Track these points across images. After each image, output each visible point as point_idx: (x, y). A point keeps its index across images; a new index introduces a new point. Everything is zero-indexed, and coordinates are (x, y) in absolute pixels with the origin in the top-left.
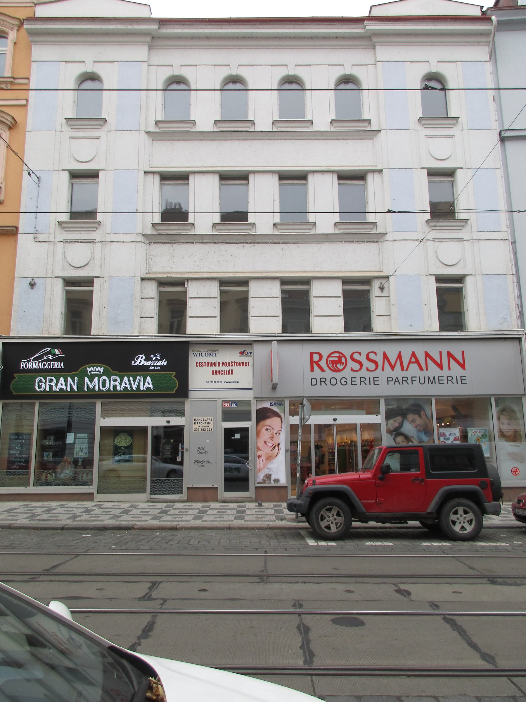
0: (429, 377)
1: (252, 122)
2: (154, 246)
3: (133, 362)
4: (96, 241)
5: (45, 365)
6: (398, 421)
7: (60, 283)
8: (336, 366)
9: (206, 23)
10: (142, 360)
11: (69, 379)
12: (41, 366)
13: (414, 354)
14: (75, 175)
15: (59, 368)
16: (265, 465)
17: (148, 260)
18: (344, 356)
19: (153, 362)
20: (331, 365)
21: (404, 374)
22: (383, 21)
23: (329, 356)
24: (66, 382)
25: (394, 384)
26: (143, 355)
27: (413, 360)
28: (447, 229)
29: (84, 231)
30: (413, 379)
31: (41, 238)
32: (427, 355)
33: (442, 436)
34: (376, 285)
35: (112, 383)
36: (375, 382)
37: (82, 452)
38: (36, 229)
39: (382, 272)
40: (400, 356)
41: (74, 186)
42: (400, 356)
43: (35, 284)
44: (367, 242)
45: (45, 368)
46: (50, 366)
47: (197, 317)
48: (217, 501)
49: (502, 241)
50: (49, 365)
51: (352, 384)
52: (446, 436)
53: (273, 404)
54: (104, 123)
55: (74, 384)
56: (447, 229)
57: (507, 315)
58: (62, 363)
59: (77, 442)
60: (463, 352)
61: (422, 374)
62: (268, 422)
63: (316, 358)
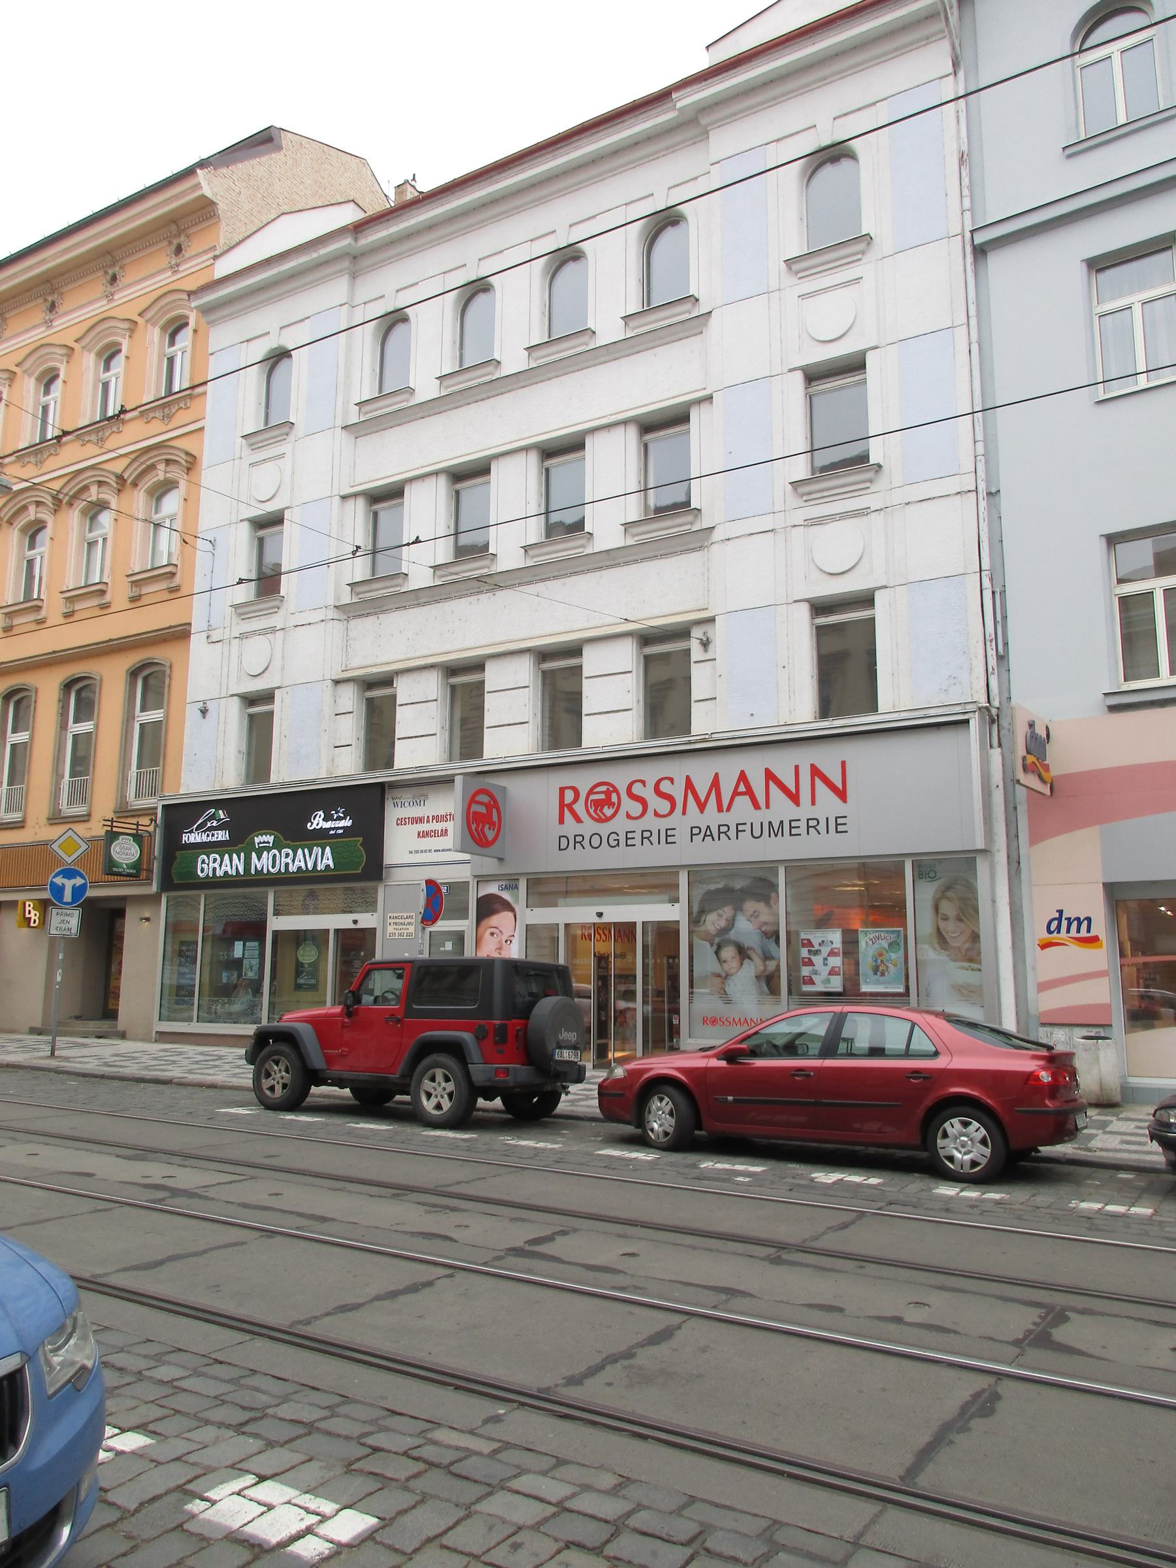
0: (770, 823)
1: (692, 298)
3: (309, 824)
4: (277, 629)
5: (208, 836)
6: (725, 916)
7: (235, 703)
8: (601, 811)
9: (419, 205)
10: (321, 820)
11: (235, 856)
13: (743, 777)
14: (813, 375)
17: (344, 650)
18: (616, 790)
20: (593, 808)
21: (724, 818)
22: (706, 80)
23: (591, 792)
25: (703, 840)
27: (742, 788)
28: (835, 495)
30: (740, 828)
32: (770, 776)
33: (804, 946)
34: (697, 633)
35: (283, 859)
36: (668, 836)
39: (707, 609)
40: (716, 784)
41: (815, 399)
42: (716, 784)
43: (207, 710)
44: (682, 552)
47: (408, 738)
49: (959, 496)
50: (213, 835)
51: (837, 832)
52: (813, 947)
53: (503, 887)
54: (291, 428)
56: (835, 495)
57: (961, 668)
59: (246, 956)
60: (843, 764)
61: (764, 816)
62: (495, 920)
63: (569, 796)
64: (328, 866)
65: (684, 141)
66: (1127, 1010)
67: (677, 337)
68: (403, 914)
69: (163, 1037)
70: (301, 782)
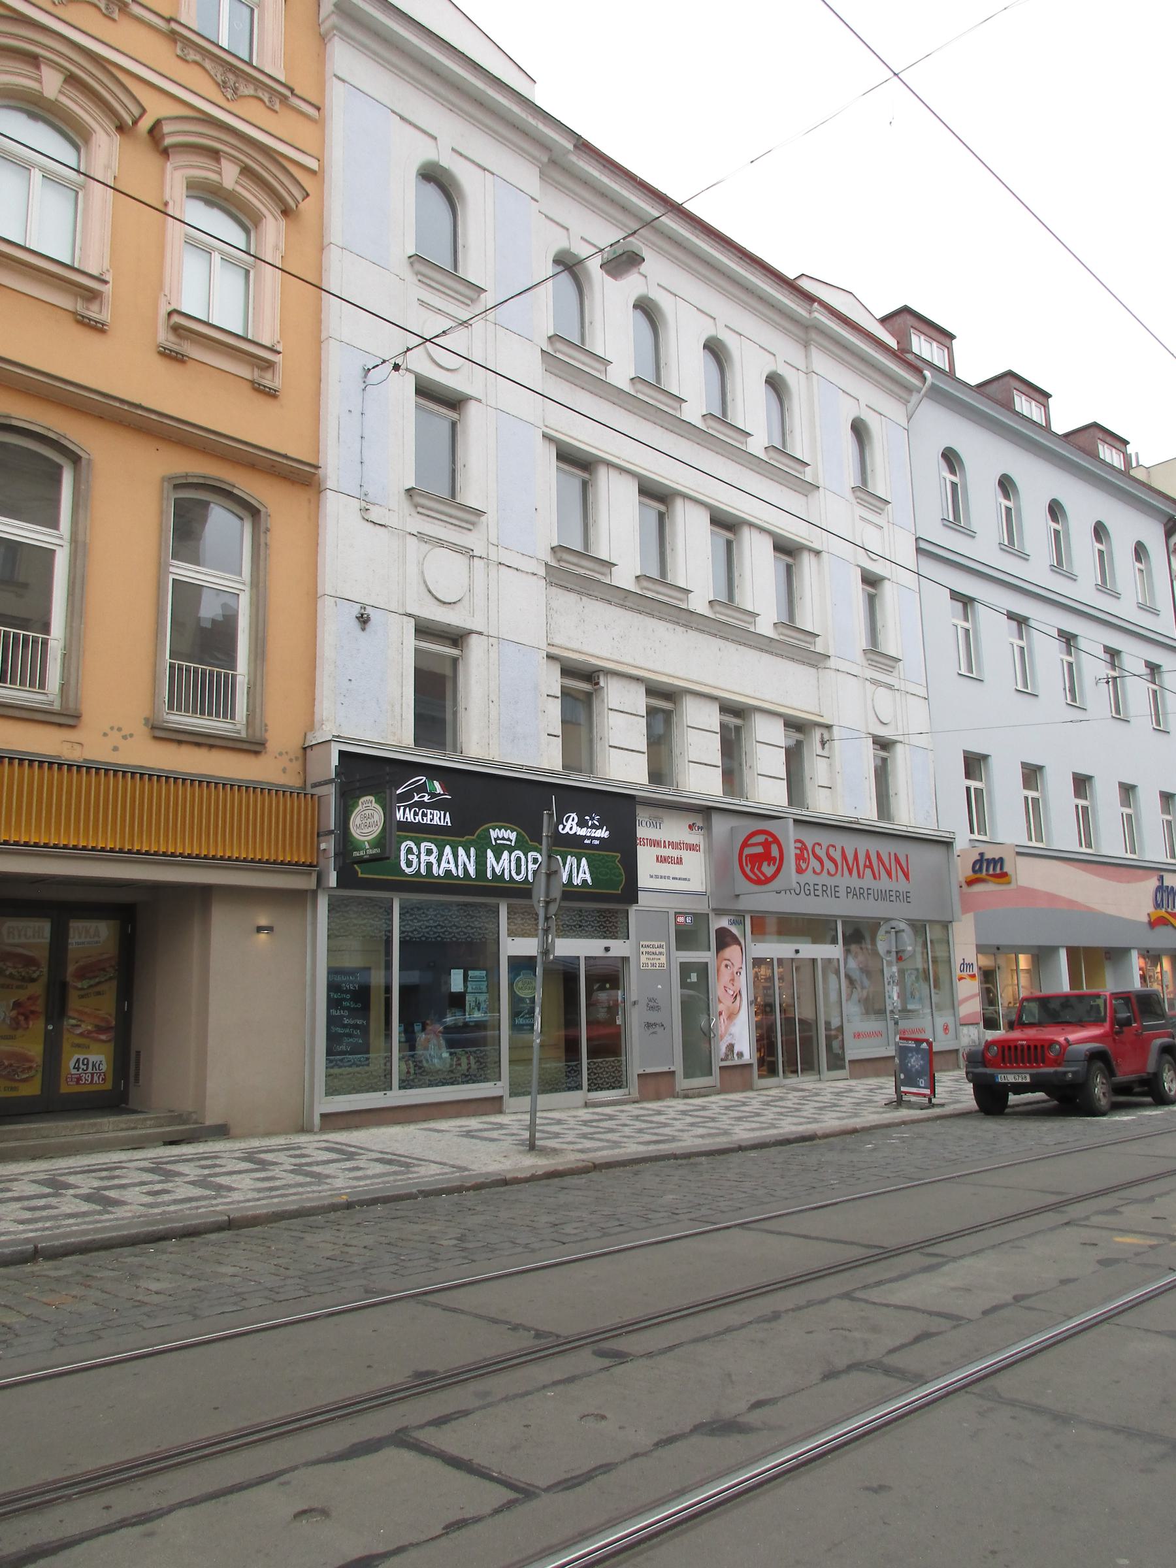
2: (554, 590)
5: (416, 814)
11: (461, 851)
12: (408, 816)
15: (442, 824)
16: (727, 1028)
18: (776, 841)
19: (589, 830)
23: (745, 844)
24: (456, 856)
26: (574, 815)
29: (452, 524)
31: (373, 516)
34: (817, 734)
37: (479, 1010)
38: (364, 489)
45: (417, 821)
46: (425, 818)
48: (675, 1096)
50: (424, 815)
55: (470, 861)
58: (448, 814)
59: (469, 990)
64: (585, 881)
65: (795, 335)
66: (486, 1021)
67: (772, 477)
68: (652, 943)
69: (332, 1121)
70: (530, 769)
